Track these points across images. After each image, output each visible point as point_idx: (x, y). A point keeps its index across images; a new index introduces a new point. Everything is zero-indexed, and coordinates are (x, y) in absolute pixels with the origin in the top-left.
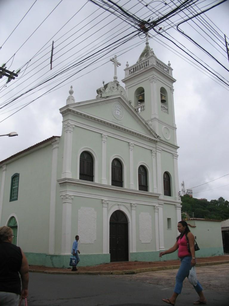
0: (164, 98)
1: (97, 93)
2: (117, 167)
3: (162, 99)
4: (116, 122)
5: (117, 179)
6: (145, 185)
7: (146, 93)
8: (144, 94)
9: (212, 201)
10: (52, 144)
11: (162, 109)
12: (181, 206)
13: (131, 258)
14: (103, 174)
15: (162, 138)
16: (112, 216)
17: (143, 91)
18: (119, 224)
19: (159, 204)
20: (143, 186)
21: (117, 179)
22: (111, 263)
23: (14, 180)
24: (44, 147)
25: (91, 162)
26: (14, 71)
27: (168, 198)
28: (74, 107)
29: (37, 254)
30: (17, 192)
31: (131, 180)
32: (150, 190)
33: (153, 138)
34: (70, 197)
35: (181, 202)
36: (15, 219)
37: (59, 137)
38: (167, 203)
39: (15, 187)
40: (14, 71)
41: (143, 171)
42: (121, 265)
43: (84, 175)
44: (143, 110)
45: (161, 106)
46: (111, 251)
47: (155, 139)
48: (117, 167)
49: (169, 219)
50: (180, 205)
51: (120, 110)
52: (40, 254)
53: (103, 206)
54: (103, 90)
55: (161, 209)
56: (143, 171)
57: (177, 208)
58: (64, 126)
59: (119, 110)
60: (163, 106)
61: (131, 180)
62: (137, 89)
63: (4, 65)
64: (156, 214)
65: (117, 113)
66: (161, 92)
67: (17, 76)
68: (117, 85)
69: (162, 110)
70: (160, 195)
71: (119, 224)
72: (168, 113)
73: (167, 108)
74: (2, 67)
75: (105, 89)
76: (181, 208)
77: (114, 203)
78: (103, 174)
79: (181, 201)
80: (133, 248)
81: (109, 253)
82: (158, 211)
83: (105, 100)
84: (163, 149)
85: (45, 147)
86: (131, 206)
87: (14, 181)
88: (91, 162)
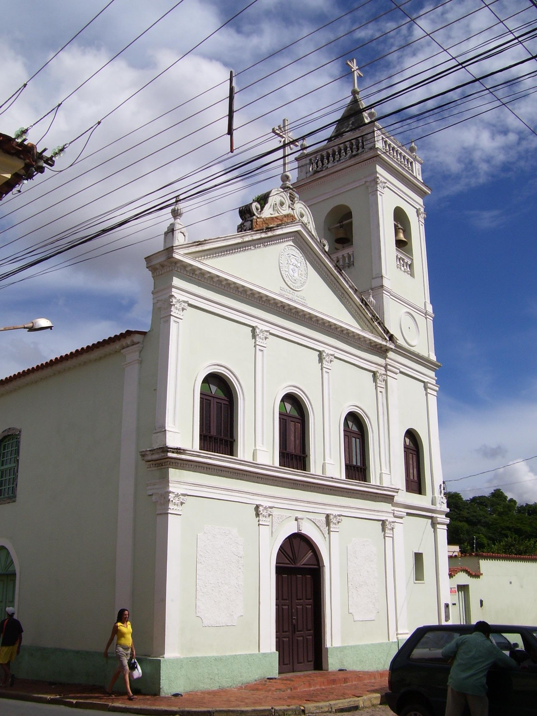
0: (401, 236)
1: (241, 217)
2: (294, 416)
3: (398, 239)
4: (290, 296)
5: (294, 451)
6: (359, 464)
7: (356, 220)
8: (351, 224)
9: (474, 500)
10: (122, 351)
11: (398, 263)
12: (447, 521)
13: (333, 663)
14: (258, 438)
15: (401, 342)
16: (282, 550)
17: (349, 215)
18: (300, 573)
19: (396, 517)
20: (356, 468)
21: (294, 451)
22: (283, 676)
23: (5, 445)
24: (95, 360)
25: (227, 403)
26: (45, 150)
27: (414, 499)
28: (186, 254)
29: (78, 652)
30: (15, 479)
31: (327, 454)
32: (374, 480)
33: (379, 341)
34: (177, 499)
35: (448, 510)
36: (8, 553)
37: (144, 333)
38: (414, 512)
39: (9, 466)
40: (45, 150)
41: (356, 428)
42: (304, 680)
43: (211, 437)
44: (349, 267)
45: (397, 256)
46: (279, 646)
47: (384, 343)
48: (294, 416)
49: (418, 557)
50: (444, 516)
51: (299, 265)
52: (87, 652)
53: (260, 523)
54: (257, 209)
55: (398, 528)
56: (356, 428)
57: (438, 526)
58: (159, 305)
59: (296, 266)
60: (400, 255)
61: (327, 454)
62: (330, 212)
63: (24, 132)
64: (389, 541)
65: (291, 272)
66: (395, 220)
67: (50, 162)
68: (290, 197)
69: (398, 267)
70: (397, 492)
71: (300, 573)
72: (412, 275)
73: (409, 263)
74: (15, 139)
75: (262, 208)
76: (448, 525)
77: (292, 512)
78: (258, 438)
79: (448, 507)
80: (335, 637)
81: (273, 649)
82: (393, 535)
83: (263, 235)
84: (402, 370)
85: (100, 358)
86: (328, 523)
87: (4, 449)
88: (227, 403)
